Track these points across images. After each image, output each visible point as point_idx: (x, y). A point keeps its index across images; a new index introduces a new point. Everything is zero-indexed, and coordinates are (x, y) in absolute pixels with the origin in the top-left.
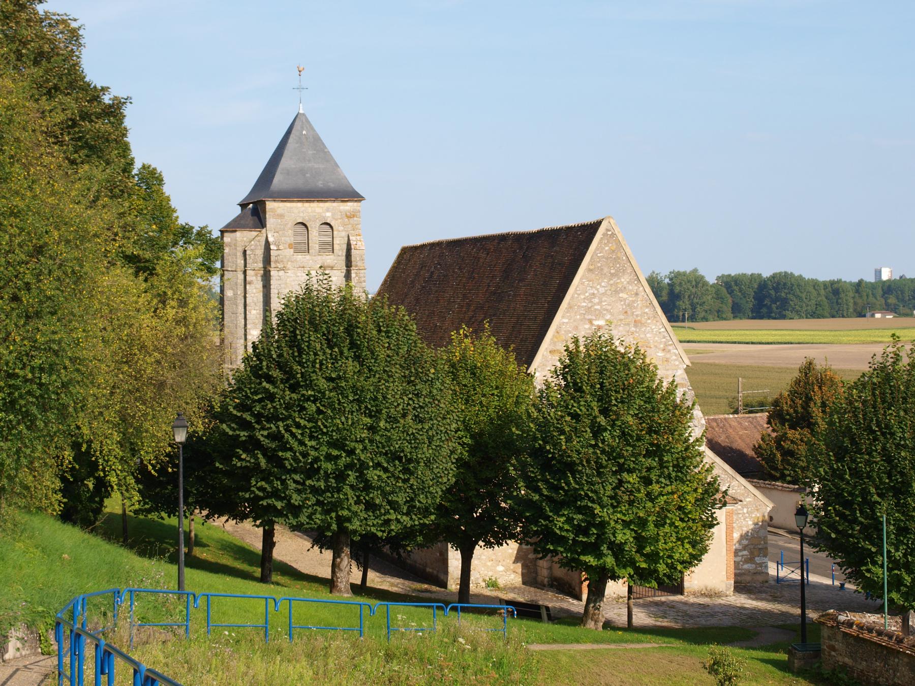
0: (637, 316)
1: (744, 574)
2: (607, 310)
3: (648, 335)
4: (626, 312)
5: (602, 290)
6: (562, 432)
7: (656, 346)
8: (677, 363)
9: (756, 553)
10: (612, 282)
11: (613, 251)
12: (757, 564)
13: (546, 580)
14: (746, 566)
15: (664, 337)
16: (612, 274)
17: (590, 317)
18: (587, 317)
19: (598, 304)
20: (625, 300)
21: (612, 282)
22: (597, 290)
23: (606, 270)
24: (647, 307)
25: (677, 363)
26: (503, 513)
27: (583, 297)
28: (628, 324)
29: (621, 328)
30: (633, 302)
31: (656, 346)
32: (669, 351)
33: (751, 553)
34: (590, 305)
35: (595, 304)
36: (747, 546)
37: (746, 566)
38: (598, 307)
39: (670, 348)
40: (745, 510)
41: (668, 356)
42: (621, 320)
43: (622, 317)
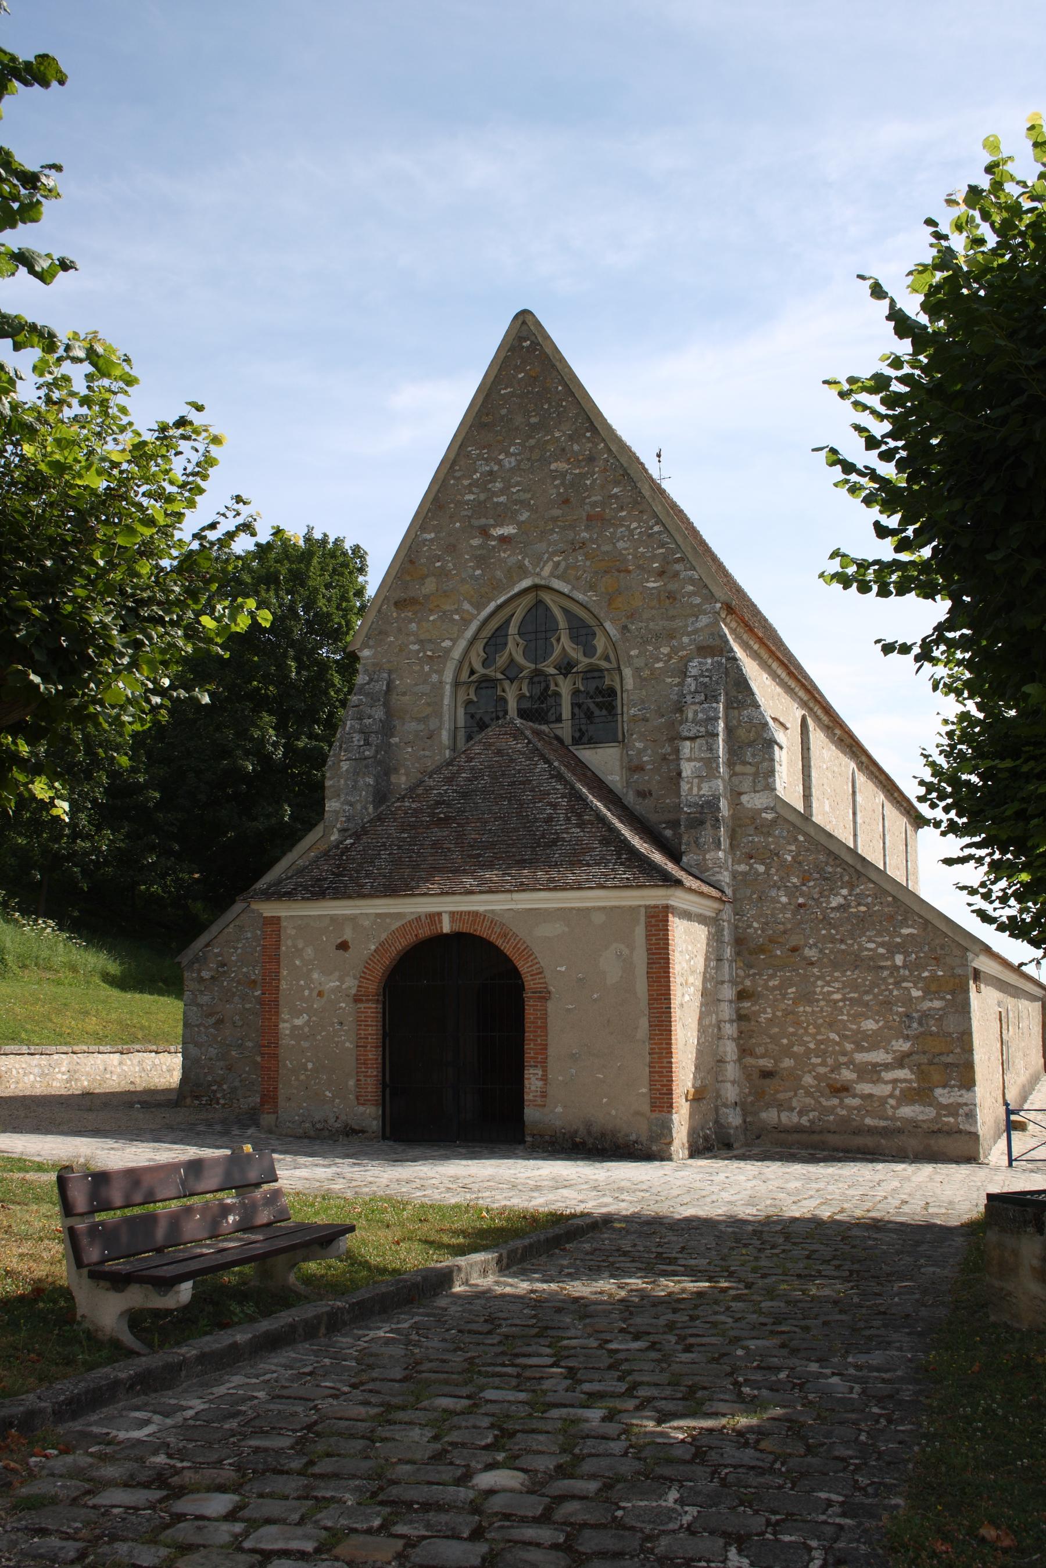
0: (594, 505)
1: (900, 1131)
2: (521, 502)
3: (620, 545)
4: (566, 501)
5: (509, 462)
6: (34, 1032)
7: (639, 567)
8: (697, 600)
9: (936, 1077)
10: (532, 442)
11: (535, 378)
12: (941, 1106)
13: (375, 1123)
14: (907, 1111)
15: (662, 545)
16: (534, 428)
17: (483, 521)
18: (476, 523)
19: (502, 492)
20: (563, 475)
21: (532, 442)
22: (499, 463)
23: (519, 420)
24: (617, 483)
25: (697, 600)
26: (563, 400)
27: (466, 482)
28: (572, 527)
29: (555, 537)
30: (583, 476)
31: (639, 567)
32: (676, 574)
33: (922, 1074)
34: (482, 497)
35: (495, 494)
36: (909, 1054)
37: (907, 1111)
38: (502, 499)
39: (678, 567)
40: (899, 960)
41: (673, 586)
42: (555, 519)
43: (556, 512)
